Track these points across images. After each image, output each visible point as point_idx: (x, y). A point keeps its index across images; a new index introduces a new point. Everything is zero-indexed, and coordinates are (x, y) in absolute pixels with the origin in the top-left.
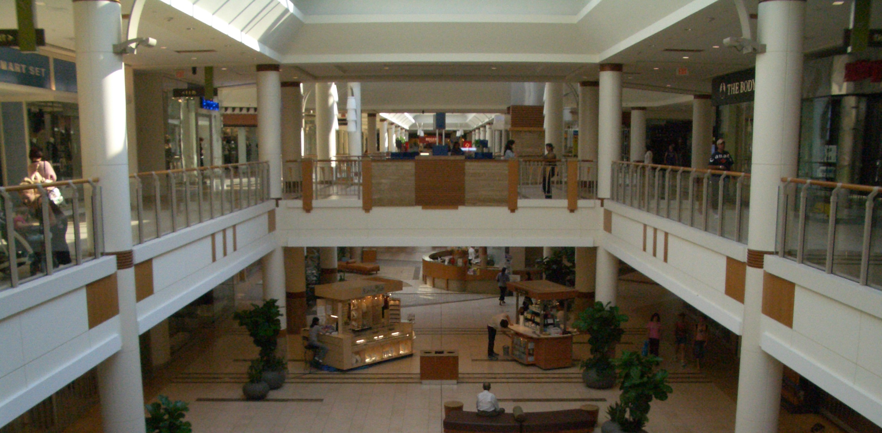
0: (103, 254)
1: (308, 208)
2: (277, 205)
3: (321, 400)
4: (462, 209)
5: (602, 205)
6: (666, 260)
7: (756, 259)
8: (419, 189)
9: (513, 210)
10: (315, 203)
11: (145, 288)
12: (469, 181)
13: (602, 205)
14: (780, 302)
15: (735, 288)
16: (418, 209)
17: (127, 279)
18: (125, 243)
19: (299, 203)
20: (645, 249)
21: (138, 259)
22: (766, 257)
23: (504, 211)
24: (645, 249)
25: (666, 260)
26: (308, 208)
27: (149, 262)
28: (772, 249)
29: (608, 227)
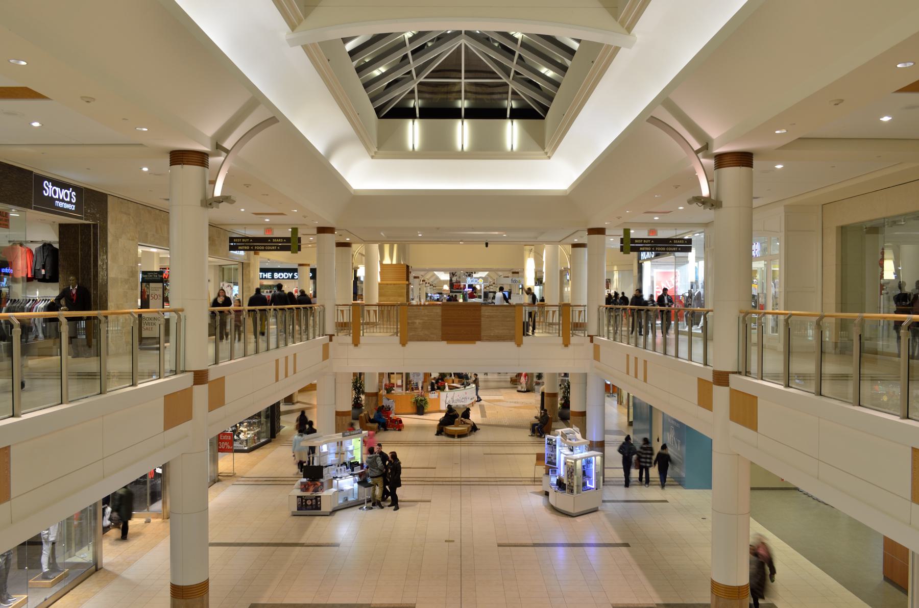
0: (183, 372)
1: (356, 343)
2: (331, 340)
3: (429, 501)
4: (478, 343)
5: (592, 341)
6: (645, 381)
7: (721, 378)
8: (445, 324)
9: (519, 345)
10: (362, 340)
11: (217, 400)
12: (484, 322)
13: (592, 341)
14: (745, 411)
15: (705, 401)
16: (444, 343)
17: (201, 393)
18: (195, 363)
19: (349, 339)
20: (645, 362)
21: (212, 377)
22: (731, 376)
23: (511, 345)
24: (645, 362)
25: (645, 381)
26: (356, 343)
27: (222, 380)
28: (736, 370)
29: (597, 357)
